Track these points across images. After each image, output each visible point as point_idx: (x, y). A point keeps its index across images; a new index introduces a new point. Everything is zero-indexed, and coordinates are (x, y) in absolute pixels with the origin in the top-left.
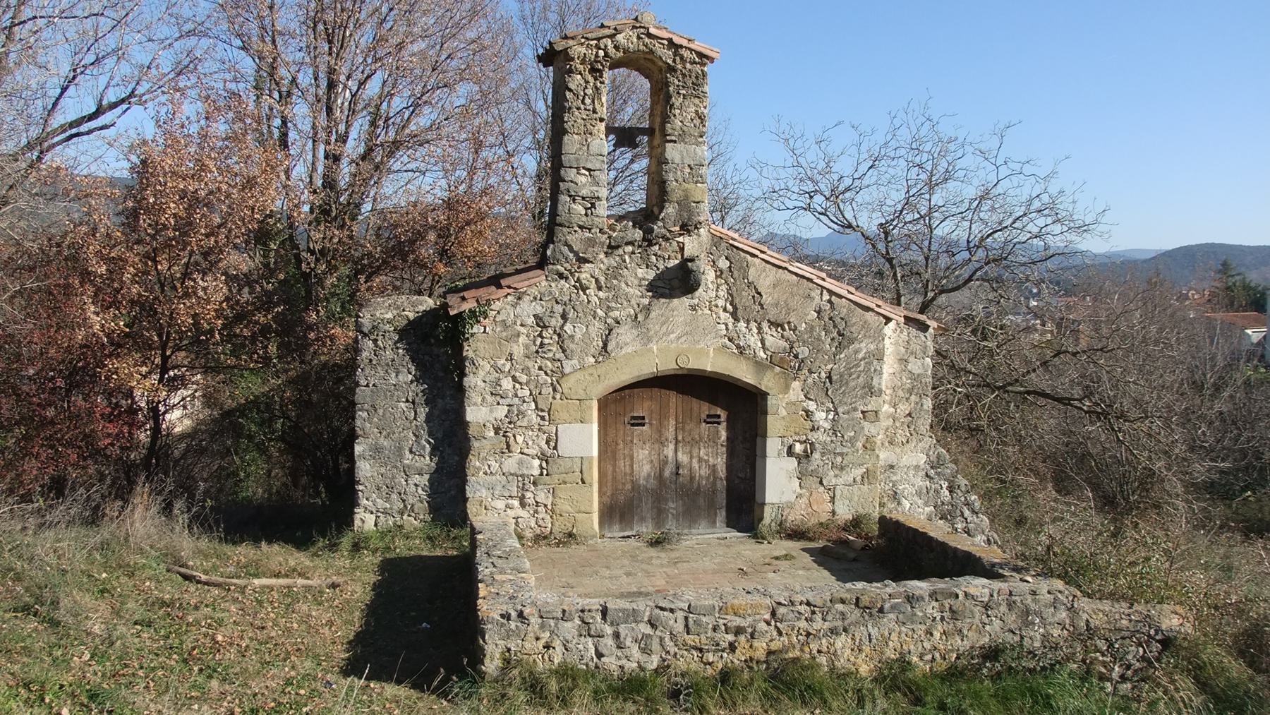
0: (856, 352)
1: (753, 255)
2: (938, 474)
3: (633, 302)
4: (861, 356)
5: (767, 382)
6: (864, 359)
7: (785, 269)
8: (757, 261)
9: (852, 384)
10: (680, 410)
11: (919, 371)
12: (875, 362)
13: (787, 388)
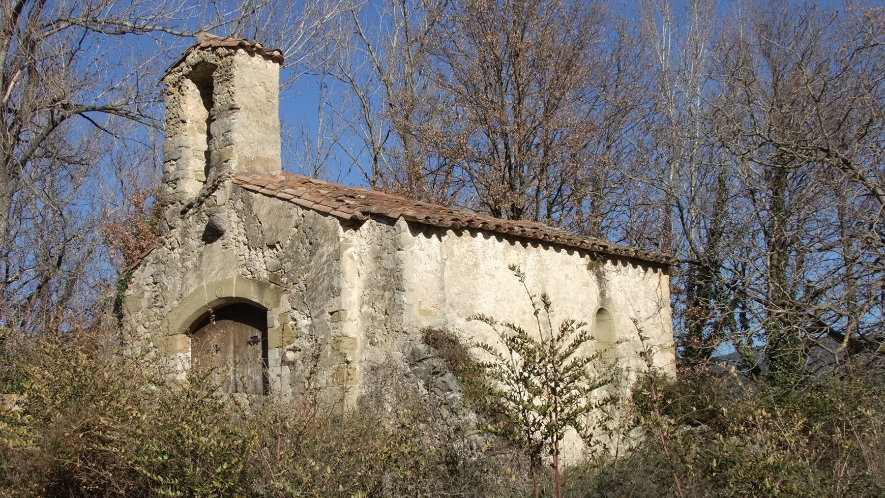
0: (321, 256)
1: (256, 192)
2: (415, 372)
3: (196, 252)
4: (324, 260)
5: (265, 301)
6: (326, 262)
7: (273, 196)
8: (258, 195)
9: (320, 288)
10: (237, 336)
11: (391, 266)
12: (335, 262)
13: (277, 303)
